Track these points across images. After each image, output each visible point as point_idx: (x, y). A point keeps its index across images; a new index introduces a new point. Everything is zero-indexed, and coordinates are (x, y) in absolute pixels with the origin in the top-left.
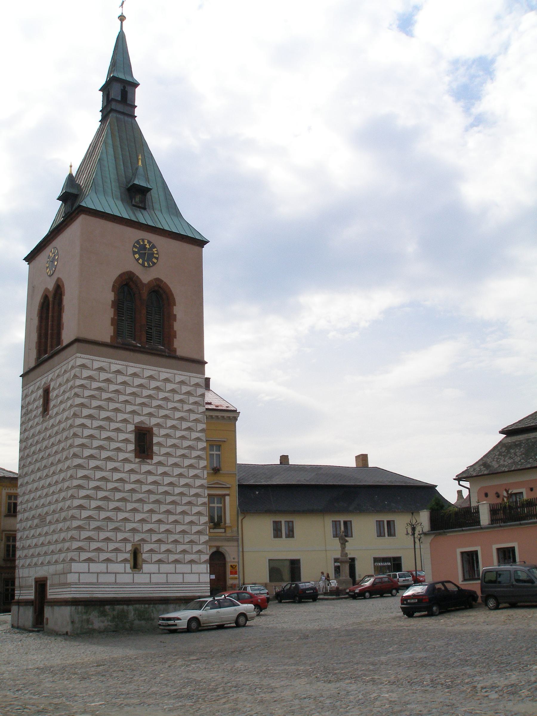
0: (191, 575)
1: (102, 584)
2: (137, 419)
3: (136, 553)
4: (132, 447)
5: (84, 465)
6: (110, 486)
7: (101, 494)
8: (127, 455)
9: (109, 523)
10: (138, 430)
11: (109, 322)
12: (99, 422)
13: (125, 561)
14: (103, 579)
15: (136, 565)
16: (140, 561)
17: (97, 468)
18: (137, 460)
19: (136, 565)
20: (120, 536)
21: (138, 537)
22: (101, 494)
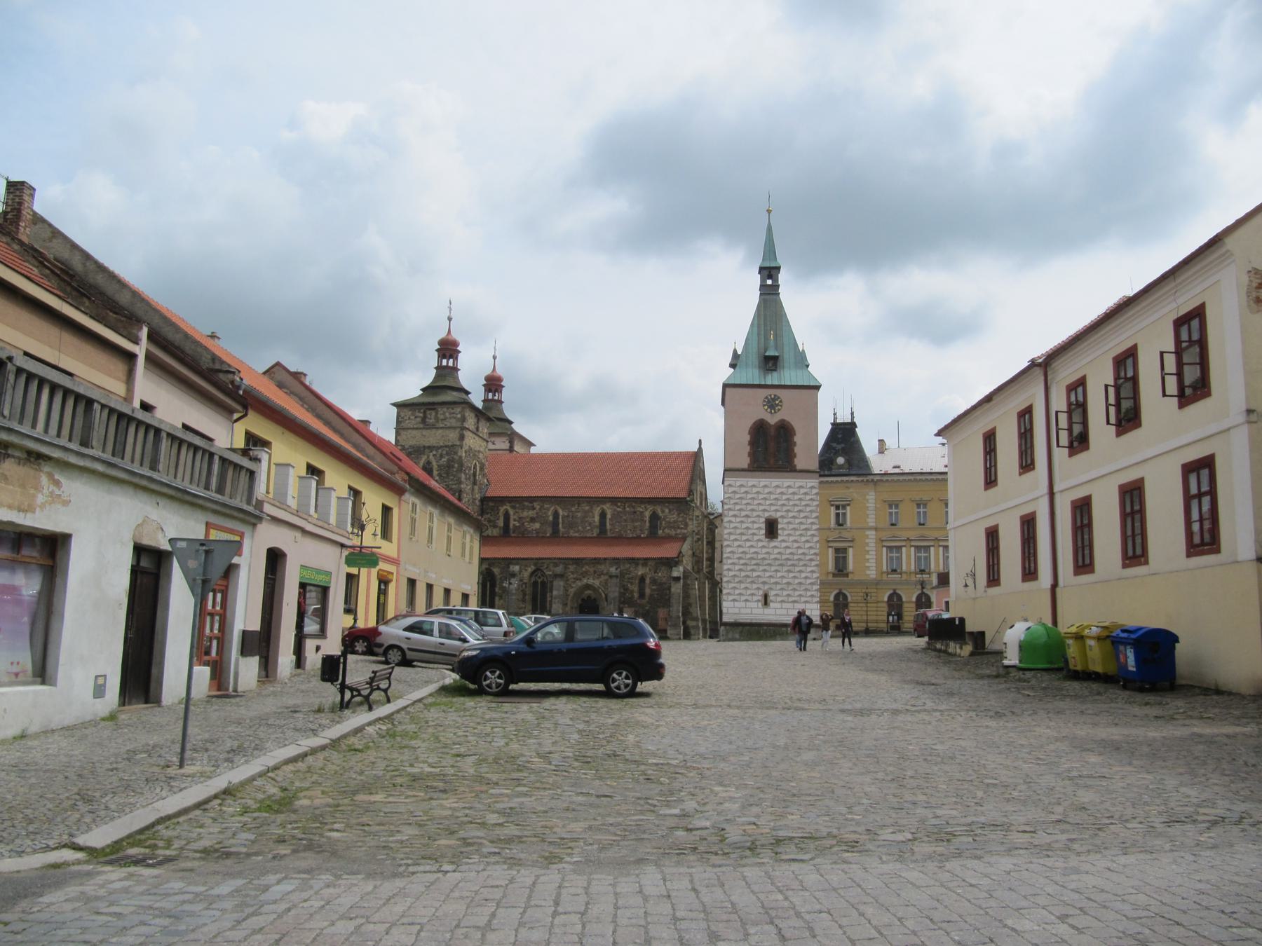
2: (767, 514)
3: (766, 596)
4: (763, 532)
6: (748, 556)
7: (742, 562)
13: (759, 601)
14: (743, 611)
15: (766, 603)
16: (768, 601)
17: (739, 546)
19: (766, 603)
20: (755, 586)
21: (766, 587)
22: (742, 562)
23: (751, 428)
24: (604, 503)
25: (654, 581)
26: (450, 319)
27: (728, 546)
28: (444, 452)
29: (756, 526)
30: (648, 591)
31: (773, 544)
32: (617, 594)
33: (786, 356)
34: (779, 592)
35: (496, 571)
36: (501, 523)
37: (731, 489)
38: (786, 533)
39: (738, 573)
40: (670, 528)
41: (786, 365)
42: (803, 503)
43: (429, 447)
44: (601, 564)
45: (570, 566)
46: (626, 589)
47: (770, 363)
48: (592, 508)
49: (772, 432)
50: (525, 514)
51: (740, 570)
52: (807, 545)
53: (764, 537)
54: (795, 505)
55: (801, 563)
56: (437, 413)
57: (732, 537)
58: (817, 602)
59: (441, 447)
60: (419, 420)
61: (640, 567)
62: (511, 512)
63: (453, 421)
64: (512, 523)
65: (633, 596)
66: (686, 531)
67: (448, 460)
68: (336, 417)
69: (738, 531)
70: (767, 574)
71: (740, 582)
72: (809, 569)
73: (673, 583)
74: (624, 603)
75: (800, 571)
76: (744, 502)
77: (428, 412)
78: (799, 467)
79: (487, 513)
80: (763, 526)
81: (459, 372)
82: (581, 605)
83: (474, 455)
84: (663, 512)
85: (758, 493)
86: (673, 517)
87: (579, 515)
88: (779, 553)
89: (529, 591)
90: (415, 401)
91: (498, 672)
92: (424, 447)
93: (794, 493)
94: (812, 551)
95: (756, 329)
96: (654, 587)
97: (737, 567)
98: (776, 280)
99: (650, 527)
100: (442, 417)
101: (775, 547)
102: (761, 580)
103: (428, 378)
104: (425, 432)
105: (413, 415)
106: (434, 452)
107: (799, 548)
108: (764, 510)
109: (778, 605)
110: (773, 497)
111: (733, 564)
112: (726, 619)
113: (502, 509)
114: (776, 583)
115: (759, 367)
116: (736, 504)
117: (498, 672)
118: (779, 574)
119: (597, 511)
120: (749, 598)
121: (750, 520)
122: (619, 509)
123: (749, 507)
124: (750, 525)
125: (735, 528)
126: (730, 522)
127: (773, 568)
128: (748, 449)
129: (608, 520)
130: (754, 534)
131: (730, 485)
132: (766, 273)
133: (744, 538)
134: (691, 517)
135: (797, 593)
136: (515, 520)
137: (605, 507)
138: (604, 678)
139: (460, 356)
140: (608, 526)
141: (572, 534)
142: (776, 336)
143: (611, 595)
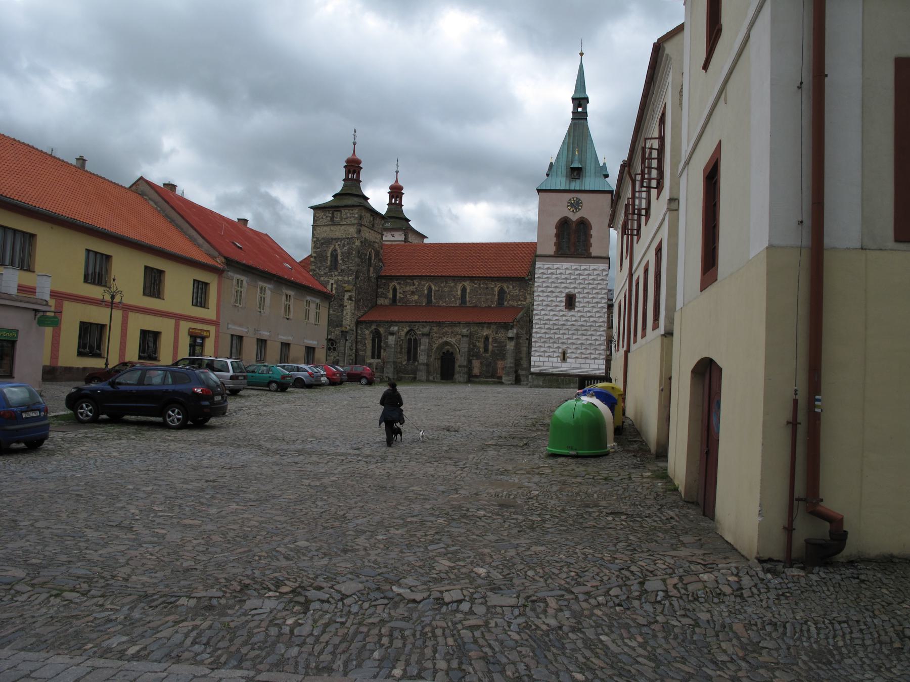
2: (567, 291)
3: (564, 353)
4: (564, 304)
6: (552, 322)
7: (547, 326)
13: (558, 357)
14: (546, 364)
20: (556, 345)
21: (565, 346)
22: (547, 326)
24: (465, 281)
25: (495, 340)
26: (355, 144)
27: (537, 314)
29: (559, 299)
30: (490, 347)
31: (571, 313)
32: (466, 349)
33: (588, 168)
34: (575, 351)
35: (382, 330)
36: (390, 295)
38: (581, 305)
39: (543, 335)
40: (513, 300)
41: (587, 174)
42: (596, 282)
43: (335, 239)
44: (456, 326)
46: (475, 346)
47: (576, 173)
48: (456, 284)
49: (574, 226)
50: (408, 288)
51: (545, 333)
52: (598, 315)
54: (589, 284)
55: (593, 328)
57: (540, 308)
58: (603, 359)
60: (329, 218)
61: (485, 329)
62: (398, 287)
63: (352, 219)
64: (398, 295)
68: (178, 216)
69: (545, 303)
70: (566, 337)
72: (598, 333)
74: (473, 356)
75: (592, 335)
76: (568, 281)
77: (335, 213)
78: (593, 254)
80: (564, 299)
82: (442, 357)
83: (370, 245)
84: (508, 288)
85: (561, 274)
86: (516, 292)
87: (446, 289)
88: (576, 321)
89: (405, 346)
90: (331, 204)
91: (90, 407)
92: (332, 239)
93: (589, 275)
94: (601, 320)
95: (566, 147)
96: (495, 345)
97: (543, 331)
98: (585, 108)
99: (499, 299)
100: (345, 216)
101: (573, 316)
102: (561, 341)
103: (339, 187)
104: (332, 228)
107: (591, 317)
108: (565, 287)
109: (573, 360)
110: (573, 277)
111: (540, 328)
112: (533, 370)
114: (573, 343)
117: (90, 407)
118: (575, 337)
123: (554, 285)
124: (554, 299)
126: (539, 296)
127: (570, 332)
128: (554, 240)
130: (557, 306)
132: (577, 102)
133: (549, 308)
135: (588, 352)
136: (400, 293)
137: (465, 284)
138: (162, 413)
139: (362, 171)
140: (468, 299)
141: (442, 304)
142: (581, 152)
143: (463, 350)
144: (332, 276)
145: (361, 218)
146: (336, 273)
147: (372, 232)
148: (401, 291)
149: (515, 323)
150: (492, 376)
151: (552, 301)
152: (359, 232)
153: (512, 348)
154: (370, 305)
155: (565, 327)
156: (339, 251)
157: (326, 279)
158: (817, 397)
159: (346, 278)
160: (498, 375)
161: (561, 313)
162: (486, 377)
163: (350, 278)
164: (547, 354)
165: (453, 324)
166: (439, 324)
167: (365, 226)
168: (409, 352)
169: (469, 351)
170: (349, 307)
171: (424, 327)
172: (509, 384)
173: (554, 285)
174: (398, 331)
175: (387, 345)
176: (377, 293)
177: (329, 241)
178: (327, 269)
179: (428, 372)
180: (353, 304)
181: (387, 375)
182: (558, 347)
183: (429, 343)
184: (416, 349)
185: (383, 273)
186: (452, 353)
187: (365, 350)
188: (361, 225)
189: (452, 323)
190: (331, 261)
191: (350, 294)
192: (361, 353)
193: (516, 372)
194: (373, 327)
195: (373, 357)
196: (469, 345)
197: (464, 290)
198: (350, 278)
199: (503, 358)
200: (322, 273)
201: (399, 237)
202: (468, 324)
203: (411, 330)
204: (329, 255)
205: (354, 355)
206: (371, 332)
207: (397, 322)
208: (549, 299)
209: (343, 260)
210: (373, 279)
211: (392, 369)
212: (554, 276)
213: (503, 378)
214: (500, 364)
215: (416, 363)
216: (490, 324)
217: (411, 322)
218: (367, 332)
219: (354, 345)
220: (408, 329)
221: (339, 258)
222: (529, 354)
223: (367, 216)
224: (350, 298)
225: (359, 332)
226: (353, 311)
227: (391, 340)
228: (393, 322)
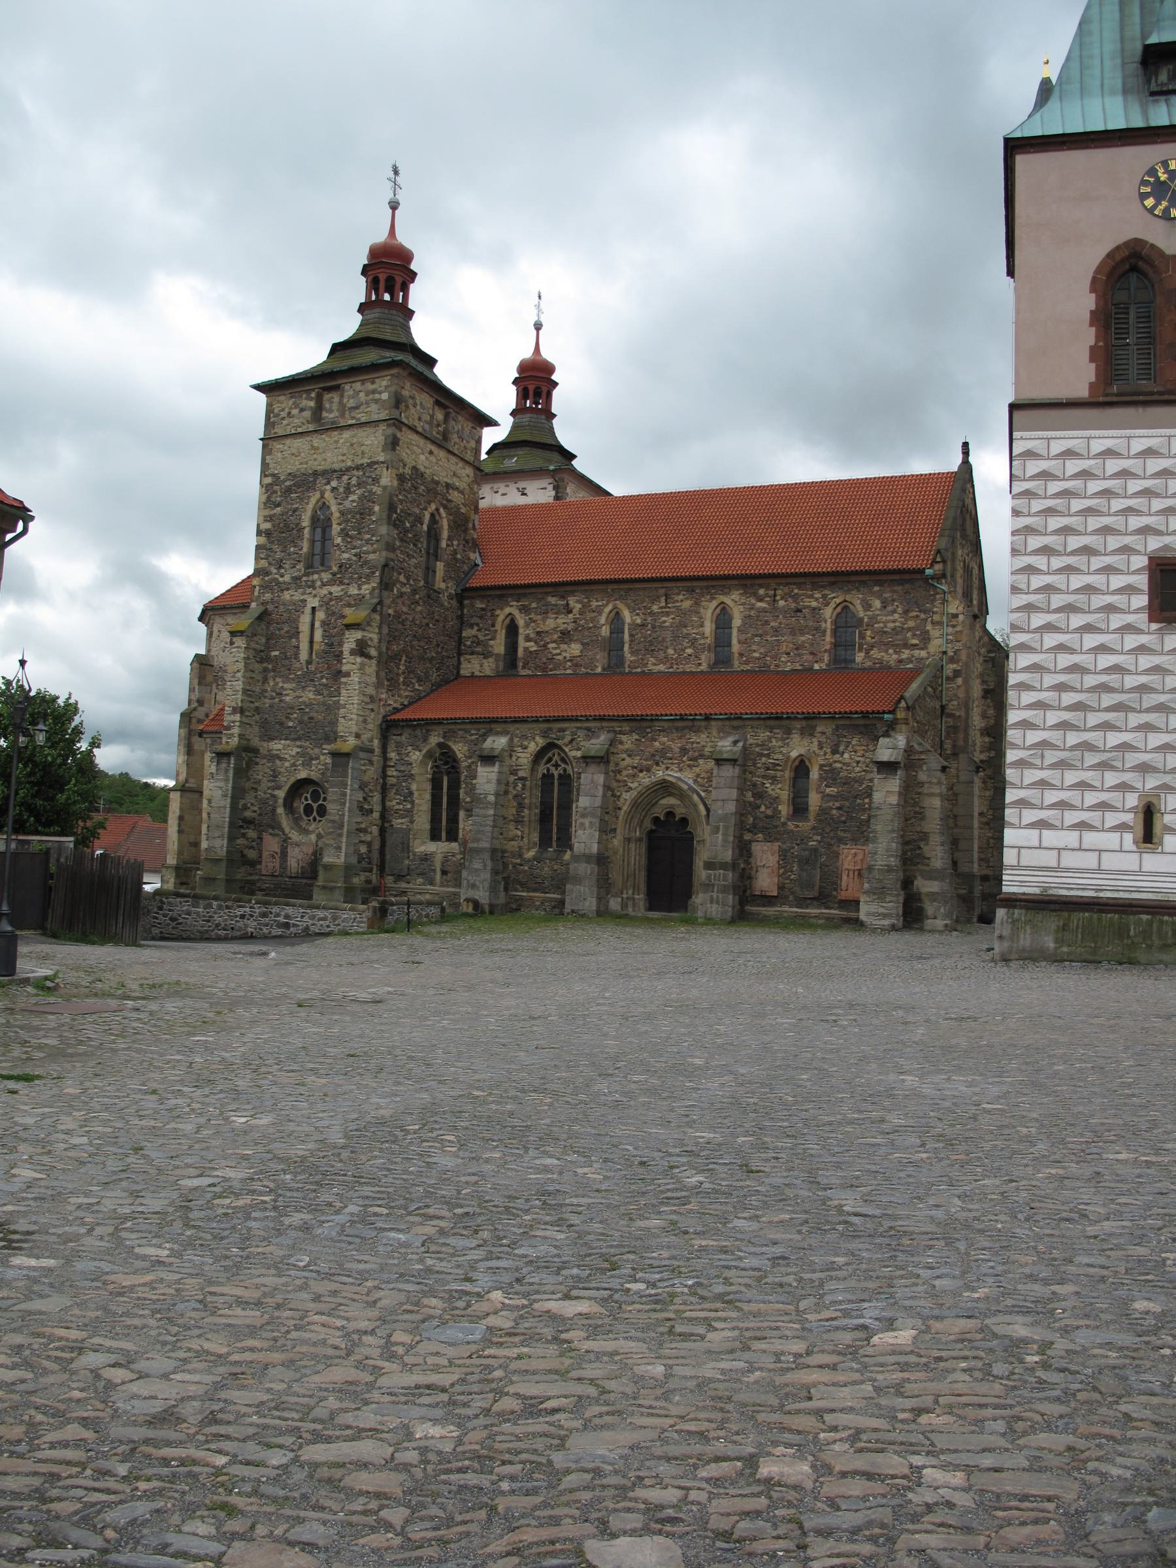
0: (1080, 853)
1: (1068, 870)
2: (1154, 544)
3: (1149, 813)
4: (1142, 600)
5: (1033, 645)
6: (1090, 681)
7: (1068, 698)
8: (1130, 618)
9: (1086, 754)
10: (1158, 565)
11: (1086, 354)
12: (1065, 558)
13: (1122, 827)
14: (1069, 860)
15: (1148, 836)
16: (1157, 829)
17: (1061, 648)
18: (1154, 626)
19: (1148, 836)
20: (1111, 779)
21: (1152, 782)
22: (1068, 698)
23: (1098, 270)
24: (726, 590)
25: (830, 774)
28: (354, 481)
29: (1117, 582)
30: (814, 800)
32: (731, 807)
35: (460, 749)
36: (499, 646)
37: (1033, 467)
44: (698, 731)
45: (624, 738)
46: (760, 795)
48: (697, 604)
50: (550, 623)
51: (1064, 726)
53: (1144, 616)
56: (342, 396)
59: (348, 469)
60: (307, 414)
61: (796, 737)
62: (521, 621)
63: (374, 407)
64: (522, 644)
65: (777, 812)
66: (923, 654)
67: (362, 498)
69: (1057, 601)
71: (1062, 765)
73: (877, 778)
74: (753, 829)
76: (1077, 505)
77: (327, 396)
79: (471, 626)
80: (1142, 581)
81: (555, 421)
82: (651, 833)
84: (867, 606)
86: (893, 619)
87: (668, 620)
89: (532, 798)
92: (315, 474)
97: (1053, 718)
100: (351, 403)
102: (1133, 759)
103: (348, 326)
104: (317, 441)
105: (296, 405)
106: (334, 484)
108: (1145, 531)
111: (1039, 705)
112: (1011, 884)
113: (501, 615)
115: (1125, 92)
116: (1050, 512)
119: (709, 610)
120: (1092, 817)
121: (1097, 562)
122: (759, 604)
124: (1097, 580)
125: (1048, 589)
128: (1089, 336)
129: (735, 632)
130: (1110, 609)
131: (1030, 454)
133: (1077, 621)
134: (936, 618)
136: (528, 639)
137: (727, 600)
140: (736, 647)
143: (718, 810)
144: (312, 586)
145: (398, 401)
146: (326, 576)
147: (442, 454)
148: (530, 632)
149: (900, 715)
150: (823, 898)
151: (1089, 589)
152: (393, 444)
153: (894, 799)
154: (434, 677)
155: (1151, 700)
156: (334, 508)
157: (298, 596)
158: (83, 745)
159: (353, 590)
160: (843, 895)
161: (1131, 641)
162: (802, 902)
163: (366, 589)
164: (1071, 817)
165: (685, 723)
166: (640, 723)
167: (413, 429)
168: (545, 818)
169: (741, 814)
170: (355, 678)
171: (591, 733)
172: (884, 930)
173: (1094, 523)
174: (511, 750)
175: (477, 800)
176: (460, 641)
177: (305, 482)
178: (300, 566)
179: (604, 885)
180: (372, 667)
181: (471, 894)
182: (1124, 787)
183: (607, 787)
184: (566, 807)
185: (474, 583)
186: (684, 821)
187: (409, 814)
188: (397, 423)
189: (682, 718)
190: (312, 542)
191: (359, 635)
192: (398, 823)
193: (907, 883)
194: (434, 740)
195: (435, 836)
196: (741, 790)
197: (723, 620)
198: (366, 589)
199: (862, 833)
200: (287, 578)
201: (539, 493)
202: (735, 721)
203: (550, 746)
204: (306, 522)
205: (375, 830)
206: (429, 755)
207: (505, 721)
208: (1077, 581)
209: (344, 533)
210: (444, 597)
211: (487, 875)
212: (1094, 486)
213: (863, 908)
214: (849, 857)
215: (567, 856)
216: (811, 718)
217: (547, 720)
218: (416, 756)
219: (377, 797)
220: (541, 742)
221: (336, 528)
222: (996, 823)
223: (422, 406)
224: (361, 649)
225: (392, 755)
226: (371, 690)
227: (486, 779)
228: (494, 721)
